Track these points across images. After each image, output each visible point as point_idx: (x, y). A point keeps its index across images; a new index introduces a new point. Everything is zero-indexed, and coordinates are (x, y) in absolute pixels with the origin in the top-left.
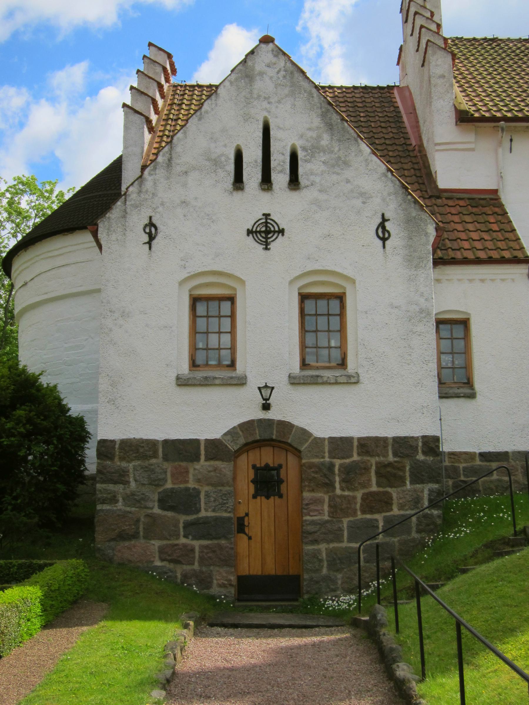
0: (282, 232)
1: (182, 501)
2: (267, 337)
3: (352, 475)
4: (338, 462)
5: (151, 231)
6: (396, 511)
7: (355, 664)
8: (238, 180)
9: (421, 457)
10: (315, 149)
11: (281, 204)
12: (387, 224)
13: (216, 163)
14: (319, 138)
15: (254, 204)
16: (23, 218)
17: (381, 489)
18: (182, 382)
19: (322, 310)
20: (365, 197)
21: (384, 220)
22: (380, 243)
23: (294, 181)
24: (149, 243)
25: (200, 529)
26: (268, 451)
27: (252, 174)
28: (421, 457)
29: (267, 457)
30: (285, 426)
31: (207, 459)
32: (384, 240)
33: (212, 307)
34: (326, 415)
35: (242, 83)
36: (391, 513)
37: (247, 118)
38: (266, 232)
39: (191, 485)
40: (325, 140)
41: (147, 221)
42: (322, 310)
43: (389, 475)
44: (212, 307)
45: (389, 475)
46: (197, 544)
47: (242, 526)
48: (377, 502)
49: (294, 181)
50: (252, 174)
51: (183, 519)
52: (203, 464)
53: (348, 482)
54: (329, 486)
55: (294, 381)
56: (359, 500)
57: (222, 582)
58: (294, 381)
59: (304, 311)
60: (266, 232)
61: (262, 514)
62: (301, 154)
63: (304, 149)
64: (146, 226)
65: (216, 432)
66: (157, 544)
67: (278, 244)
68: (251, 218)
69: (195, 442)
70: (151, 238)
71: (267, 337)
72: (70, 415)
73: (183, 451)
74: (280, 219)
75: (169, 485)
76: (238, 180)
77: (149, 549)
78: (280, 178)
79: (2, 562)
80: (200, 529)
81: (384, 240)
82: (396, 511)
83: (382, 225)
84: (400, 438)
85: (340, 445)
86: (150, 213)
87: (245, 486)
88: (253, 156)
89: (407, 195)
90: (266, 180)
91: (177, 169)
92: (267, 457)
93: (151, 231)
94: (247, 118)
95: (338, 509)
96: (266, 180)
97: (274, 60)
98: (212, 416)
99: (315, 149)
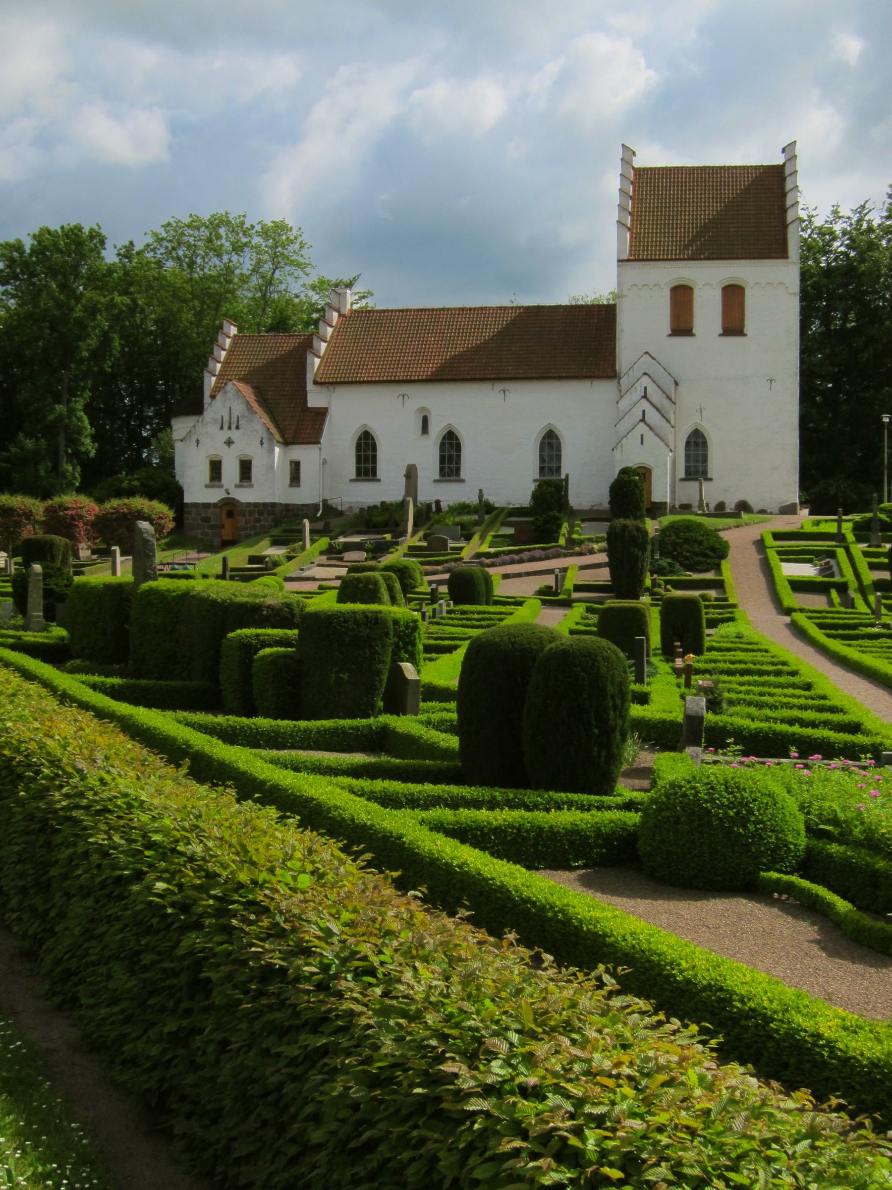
1: (206, 520)
2: (231, 472)
3: (251, 513)
7: (280, 1086)
8: (222, 428)
10: (243, 416)
11: (234, 434)
13: (216, 421)
15: (226, 434)
18: (207, 486)
19: (246, 468)
20: (257, 431)
23: (237, 428)
25: (212, 527)
26: (229, 506)
27: (226, 426)
30: (234, 499)
33: (216, 467)
34: (245, 496)
38: (229, 442)
40: (247, 413)
42: (246, 468)
44: (216, 467)
45: (261, 513)
47: (223, 526)
48: (257, 520)
49: (237, 428)
50: (226, 426)
52: (212, 510)
55: (237, 486)
57: (217, 542)
58: (237, 486)
60: (229, 442)
61: (227, 522)
65: (215, 501)
67: (232, 446)
68: (225, 439)
71: (231, 472)
72: (127, 253)
73: (206, 506)
76: (222, 428)
77: (198, 533)
78: (233, 426)
79: (32, 57)
80: (212, 527)
87: (224, 515)
88: (226, 418)
90: (230, 428)
92: (230, 508)
95: (247, 522)
96: (230, 428)
98: (214, 496)
99: (243, 416)
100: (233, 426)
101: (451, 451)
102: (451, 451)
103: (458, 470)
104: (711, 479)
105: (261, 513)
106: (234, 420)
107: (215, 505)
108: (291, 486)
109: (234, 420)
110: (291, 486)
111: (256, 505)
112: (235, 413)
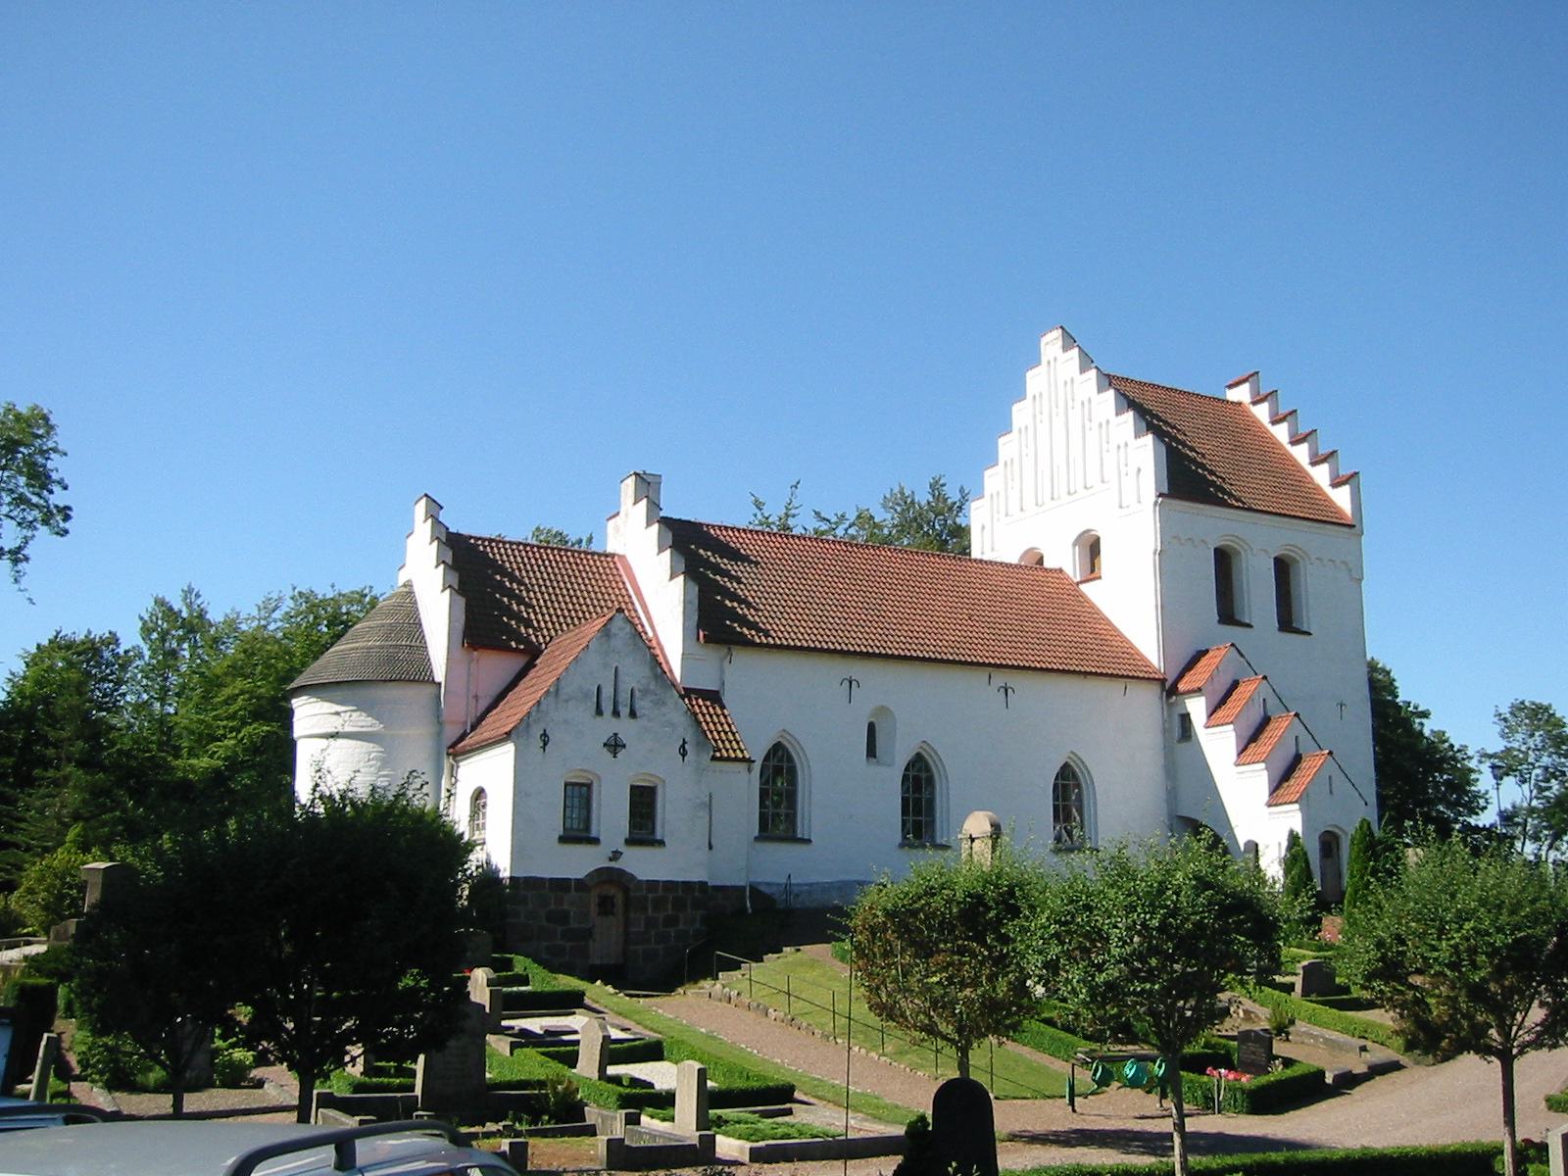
0: (624, 746)
2: (612, 816)
3: (658, 904)
4: (650, 895)
5: (545, 739)
6: (681, 926)
8: (599, 712)
9: (697, 894)
10: (645, 692)
11: (625, 728)
12: (686, 746)
13: (586, 696)
14: (648, 685)
15: (608, 726)
16: (1488, 803)
17: (668, 930)
19: (643, 801)
21: (684, 742)
22: (681, 758)
23: (633, 714)
24: (544, 748)
27: (607, 707)
28: (697, 894)
29: (612, 891)
31: (576, 890)
32: (684, 755)
34: (644, 865)
35: (604, 639)
36: (584, 1124)
37: (606, 666)
39: (566, 907)
40: (652, 686)
41: (542, 732)
42: (643, 801)
43: (679, 905)
46: (568, 945)
48: (672, 921)
49: (633, 714)
50: (607, 707)
51: (560, 929)
53: (656, 908)
54: (645, 909)
56: (661, 920)
59: (13, 1046)
60: (614, 746)
62: (637, 694)
63: (640, 691)
64: (541, 736)
65: (581, 875)
66: (545, 944)
69: (567, 880)
70: (545, 744)
73: (561, 885)
74: (623, 737)
75: (553, 907)
76: (599, 712)
78: (625, 711)
81: (684, 755)
82: (681, 926)
83: (683, 746)
84: (689, 882)
85: (652, 885)
86: (543, 726)
87: (594, 909)
88: (608, 692)
89: (284, 634)
90: (616, 713)
91: (562, 697)
93: (545, 739)
94: (606, 666)
96: (616, 713)
97: (624, 625)
99: (645, 692)
100: (625, 711)
101: (919, 790)
102: (919, 790)
103: (791, 819)
104: (661, 843)
105: (679, 905)
106: (624, 697)
107: (580, 884)
108: (905, 844)
109: (624, 697)
110: (905, 844)
111: (670, 885)
112: (628, 683)
